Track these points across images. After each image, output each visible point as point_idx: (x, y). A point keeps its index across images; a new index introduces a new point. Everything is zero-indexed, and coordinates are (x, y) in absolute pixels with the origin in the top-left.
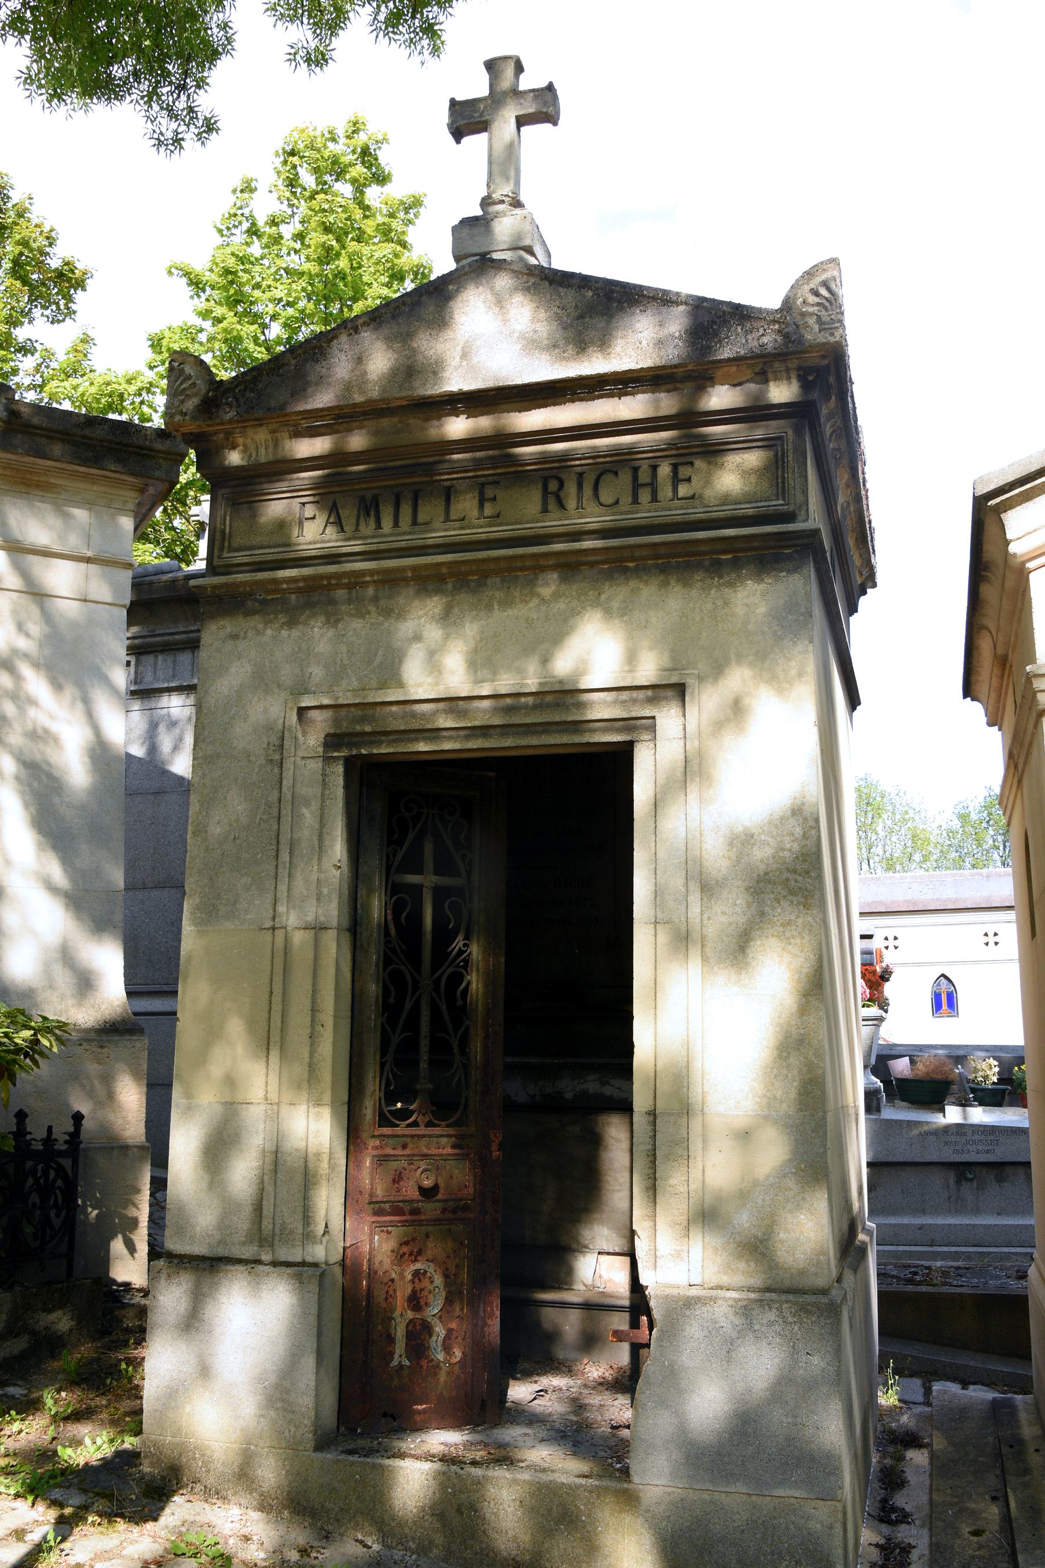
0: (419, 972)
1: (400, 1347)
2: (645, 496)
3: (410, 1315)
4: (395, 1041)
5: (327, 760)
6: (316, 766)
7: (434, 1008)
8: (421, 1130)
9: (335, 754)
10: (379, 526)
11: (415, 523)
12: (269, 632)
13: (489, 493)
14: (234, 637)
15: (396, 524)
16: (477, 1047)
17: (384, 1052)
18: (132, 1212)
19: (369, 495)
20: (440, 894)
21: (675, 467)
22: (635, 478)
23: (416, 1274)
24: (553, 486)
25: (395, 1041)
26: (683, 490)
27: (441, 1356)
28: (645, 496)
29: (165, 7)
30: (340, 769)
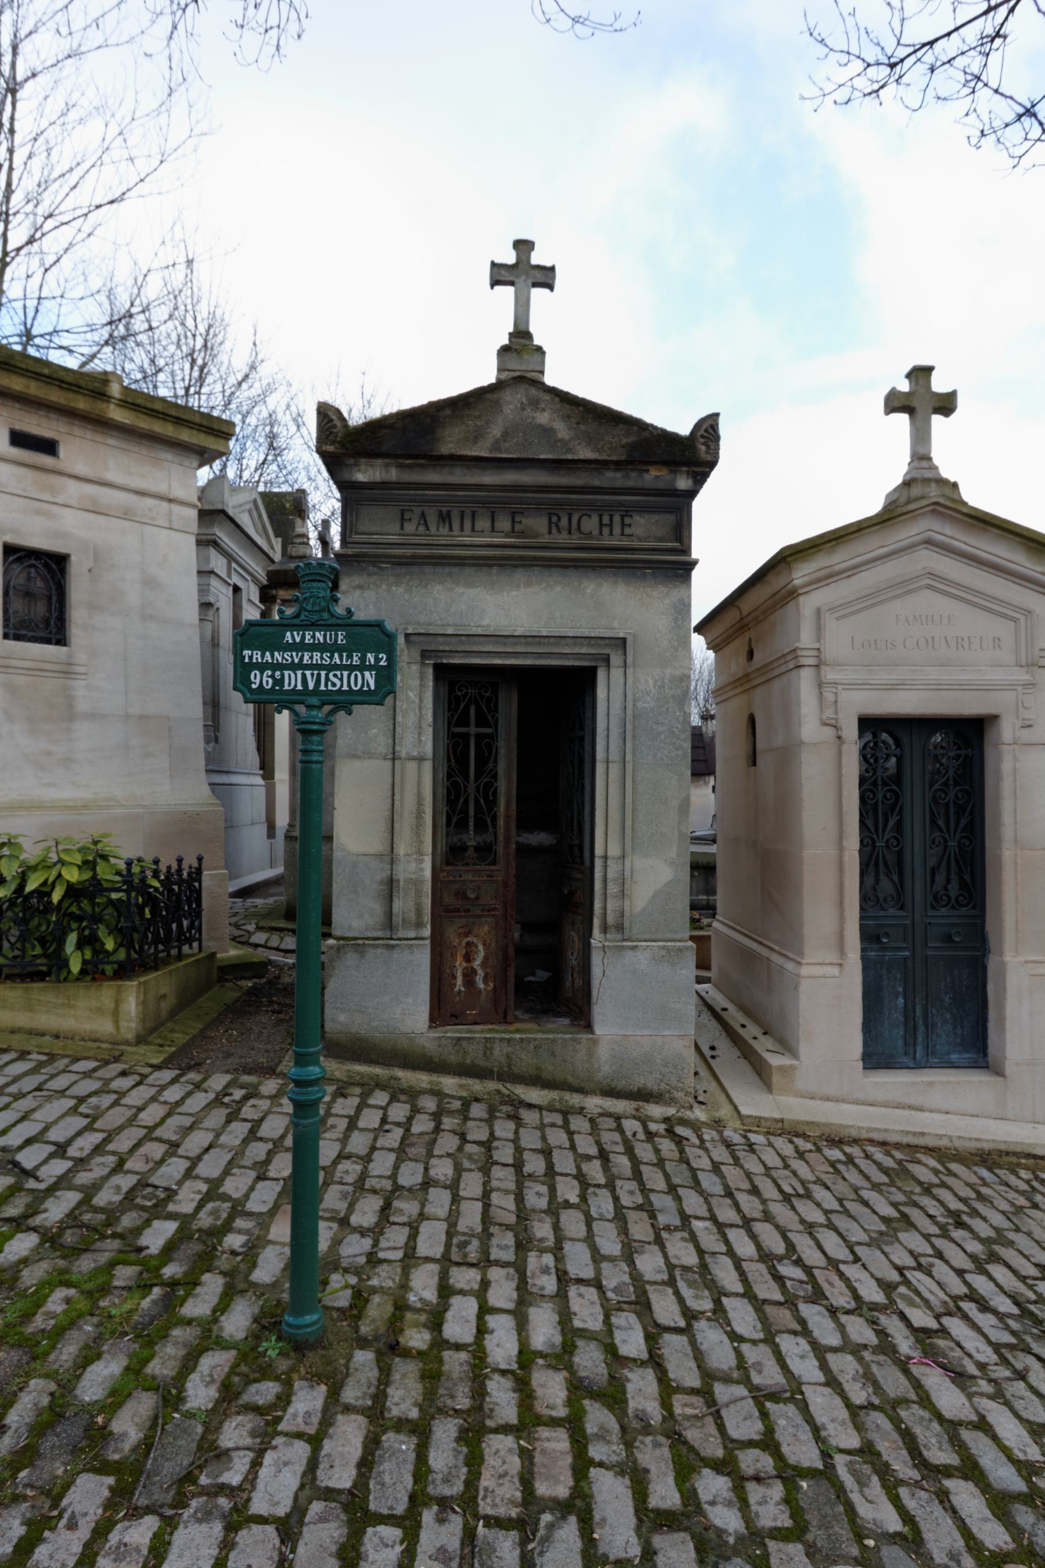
0: (468, 781)
1: (459, 980)
2: (606, 531)
3: (464, 964)
4: (454, 820)
5: (423, 664)
6: (415, 668)
7: (477, 800)
8: (470, 868)
9: (667, 1033)
10: (451, 530)
11: (473, 530)
12: (384, 587)
13: (517, 519)
14: (360, 587)
15: (462, 530)
16: (501, 822)
17: (448, 825)
18: (280, 540)
19: (444, 510)
20: (479, 737)
21: (622, 517)
22: (601, 520)
23: (468, 944)
24: (554, 519)
25: (454, 820)
26: (627, 531)
27: (482, 986)
28: (606, 531)
29: (156, 948)
30: (430, 671)
